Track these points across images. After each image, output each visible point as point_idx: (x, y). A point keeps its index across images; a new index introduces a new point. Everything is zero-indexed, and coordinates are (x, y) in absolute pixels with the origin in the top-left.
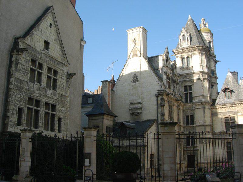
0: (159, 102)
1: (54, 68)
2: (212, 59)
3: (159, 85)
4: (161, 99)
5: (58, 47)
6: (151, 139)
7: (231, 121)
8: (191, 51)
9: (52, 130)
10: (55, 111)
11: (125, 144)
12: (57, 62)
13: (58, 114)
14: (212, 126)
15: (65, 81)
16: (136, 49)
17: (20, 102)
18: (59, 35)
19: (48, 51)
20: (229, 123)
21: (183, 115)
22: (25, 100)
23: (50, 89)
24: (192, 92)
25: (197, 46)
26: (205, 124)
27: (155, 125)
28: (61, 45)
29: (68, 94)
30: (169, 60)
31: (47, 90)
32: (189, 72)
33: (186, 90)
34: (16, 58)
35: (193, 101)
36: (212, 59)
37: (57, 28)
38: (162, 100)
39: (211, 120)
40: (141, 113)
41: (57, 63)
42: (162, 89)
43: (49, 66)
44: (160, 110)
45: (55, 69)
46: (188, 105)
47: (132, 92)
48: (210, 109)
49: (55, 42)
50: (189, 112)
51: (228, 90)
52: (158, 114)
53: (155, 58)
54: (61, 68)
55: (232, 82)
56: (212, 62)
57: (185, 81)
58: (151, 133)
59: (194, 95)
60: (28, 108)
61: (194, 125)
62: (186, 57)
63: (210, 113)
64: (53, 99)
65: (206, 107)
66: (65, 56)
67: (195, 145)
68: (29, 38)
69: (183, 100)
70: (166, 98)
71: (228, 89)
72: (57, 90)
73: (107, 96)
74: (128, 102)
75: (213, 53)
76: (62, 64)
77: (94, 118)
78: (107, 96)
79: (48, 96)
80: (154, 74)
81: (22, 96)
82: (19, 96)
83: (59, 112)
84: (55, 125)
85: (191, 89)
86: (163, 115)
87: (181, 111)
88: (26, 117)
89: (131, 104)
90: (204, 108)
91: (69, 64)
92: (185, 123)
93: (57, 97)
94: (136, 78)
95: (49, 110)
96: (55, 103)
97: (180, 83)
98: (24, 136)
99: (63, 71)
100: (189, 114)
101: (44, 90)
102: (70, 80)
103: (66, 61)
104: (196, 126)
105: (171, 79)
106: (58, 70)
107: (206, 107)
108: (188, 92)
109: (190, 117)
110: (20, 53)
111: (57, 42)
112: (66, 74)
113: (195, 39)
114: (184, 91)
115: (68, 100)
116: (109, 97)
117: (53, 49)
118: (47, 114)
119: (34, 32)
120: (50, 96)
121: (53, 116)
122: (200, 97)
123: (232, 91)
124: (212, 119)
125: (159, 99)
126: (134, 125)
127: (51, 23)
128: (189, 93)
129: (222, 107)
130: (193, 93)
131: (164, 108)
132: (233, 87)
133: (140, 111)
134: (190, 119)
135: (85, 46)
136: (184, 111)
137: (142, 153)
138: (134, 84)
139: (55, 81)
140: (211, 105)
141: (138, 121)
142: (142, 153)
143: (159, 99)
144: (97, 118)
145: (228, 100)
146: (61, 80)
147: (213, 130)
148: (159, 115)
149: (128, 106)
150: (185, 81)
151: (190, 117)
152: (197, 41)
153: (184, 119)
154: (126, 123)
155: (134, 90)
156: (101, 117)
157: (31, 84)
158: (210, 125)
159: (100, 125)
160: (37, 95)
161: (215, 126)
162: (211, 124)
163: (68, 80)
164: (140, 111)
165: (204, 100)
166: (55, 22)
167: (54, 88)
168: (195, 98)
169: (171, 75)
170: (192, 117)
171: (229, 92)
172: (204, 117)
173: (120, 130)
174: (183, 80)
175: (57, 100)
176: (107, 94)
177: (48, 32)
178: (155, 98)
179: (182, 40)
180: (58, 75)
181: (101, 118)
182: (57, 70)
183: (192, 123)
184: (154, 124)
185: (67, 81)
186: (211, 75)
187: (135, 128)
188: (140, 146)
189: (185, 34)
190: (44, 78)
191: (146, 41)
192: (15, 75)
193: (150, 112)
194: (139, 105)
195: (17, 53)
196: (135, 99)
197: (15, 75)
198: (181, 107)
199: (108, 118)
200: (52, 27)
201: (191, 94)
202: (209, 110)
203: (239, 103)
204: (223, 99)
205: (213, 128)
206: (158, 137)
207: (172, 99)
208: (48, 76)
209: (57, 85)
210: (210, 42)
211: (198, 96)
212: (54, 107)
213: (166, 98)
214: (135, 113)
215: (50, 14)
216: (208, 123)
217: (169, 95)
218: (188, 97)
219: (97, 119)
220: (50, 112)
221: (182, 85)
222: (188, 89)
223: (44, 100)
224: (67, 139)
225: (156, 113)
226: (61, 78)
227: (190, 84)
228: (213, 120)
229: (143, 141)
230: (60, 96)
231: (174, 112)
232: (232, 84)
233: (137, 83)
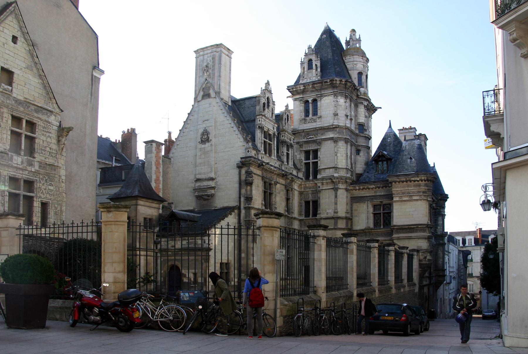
0: (243, 178)
1: (25, 118)
2: (362, 103)
3: (244, 148)
4: (247, 172)
5: (34, 81)
6: (228, 235)
7: (383, 210)
10: (33, 192)
12: (33, 108)
13: (40, 197)
14: (349, 219)
15: (54, 141)
16: (209, 85)
18: (36, 59)
19: (10, 88)
20: (380, 213)
21: (300, 200)
23: (20, 155)
24: (317, 162)
26: (335, 215)
27: (232, 216)
28: (42, 76)
29: (61, 162)
30: (271, 104)
31: (12, 156)
32: (315, 127)
33: (307, 158)
35: (319, 177)
36: (362, 103)
38: (249, 174)
39: (349, 211)
40: (212, 196)
41: (33, 109)
43: (14, 114)
44: (243, 191)
45: (27, 119)
46: (310, 184)
48: (347, 190)
49: (27, 70)
50: (310, 195)
52: (240, 198)
53: (246, 101)
54: (44, 117)
55: (394, 144)
57: (307, 142)
59: (321, 166)
61: (318, 217)
62: (310, 100)
63: (347, 197)
65: (341, 186)
66: (51, 96)
69: (301, 175)
70: (253, 169)
72: (36, 155)
73: (154, 168)
74: (192, 177)
75: (366, 94)
76: (44, 111)
78: (154, 168)
79: (16, 165)
80: (237, 131)
83: (42, 193)
84: (34, 214)
85: (316, 156)
86: (249, 199)
87: (296, 193)
89: (198, 180)
90: (336, 189)
91: (62, 111)
92: (303, 213)
93: (37, 167)
94: (206, 137)
95: (19, 190)
96: (31, 178)
97: (295, 146)
100: (310, 198)
101: (5, 155)
102: (64, 139)
103: (55, 105)
104: (321, 219)
105: (274, 137)
106: (35, 120)
107: (341, 186)
108: (311, 161)
109: (311, 204)
111: (32, 70)
112: (56, 128)
114: (303, 159)
115: (63, 172)
116: (157, 168)
117: (23, 84)
120: (20, 166)
121: (29, 200)
122: (331, 170)
124: (352, 208)
125: (243, 171)
126: (198, 215)
127: (15, 35)
128: (313, 163)
130: (319, 162)
131: (251, 187)
132: (393, 153)
133: (213, 191)
134: (311, 207)
135: (103, 79)
136: (301, 193)
138: (203, 146)
139: (31, 140)
140: (351, 184)
141: (208, 209)
143: (243, 171)
145: (382, 177)
146: (45, 139)
147: (352, 225)
148: (242, 199)
151: (311, 204)
153: (300, 206)
154: (181, 212)
155: (203, 156)
156: (134, 202)
158: (346, 218)
161: (355, 219)
162: (349, 216)
164: (213, 191)
165: (336, 175)
166: (25, 34)
167: (31, 151)
169: (275, 130)
170: (316, 204)
172: (336, 204)
173: (170, 223)
174: (304, 140)
175: (37, 173)
176: (153, 163)
177: (7, 52)
178: (236, 171)
180: (37, 130)
181: (134, 204)
182: (34, 122)
183: (315, 214)
184: (231, 214)
185: (59, 141)
186: (357, 132)
188: (202, 249)
191: (230, 70)
193: (227, 195)
196: (204, 172)
198: (296, 187)
199: (148, 204)
200: (19, 43)
201: (316, 164)
202: (345, 193)
204: (373, 174)
205: (352, 222)
207: (273, 173)
208: (13, 132)
209: (36, 147)
212: (29, 184)
213: (253, 169)
214: (204, 196)
215: (10, 18)
216: (342, 213)
217: (262, 165)
218: (311, 170)
220: (22, 192)
221: (301, 149)
222: (311, 156)
224: (47, 235)
225: (238, 196)
226: (43, 135)
227: (308, 149)
228: (353, 209)
230: (42, 165)
231: (278, 195)
232: (392, 149)
233: (207, 144)
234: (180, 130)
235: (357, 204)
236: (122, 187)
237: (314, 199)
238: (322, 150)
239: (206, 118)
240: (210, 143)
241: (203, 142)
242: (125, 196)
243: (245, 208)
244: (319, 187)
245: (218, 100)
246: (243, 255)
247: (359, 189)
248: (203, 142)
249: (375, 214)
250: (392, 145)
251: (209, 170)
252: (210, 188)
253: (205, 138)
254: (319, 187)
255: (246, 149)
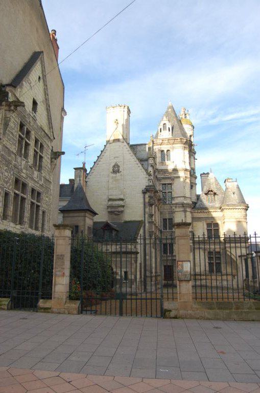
0: (147, 200)
8: (173, 144)
9: (36, 229)
11: (110, 250)
15: (49, 161)
17: (7, 183)
20: (211, 230)
21: (161, 217)
22: (12, 181)
25: (181, 139)
34: (5, 116)
36: (192, 155)
37: (45, 85)
40: (122, 212)
42: (151, 184)
44: (147, 210)
47: (111, 186)
48: (191, 212)
51: (212, 193)
52: (145, 215)
56: (192, 159)
58: (255, 234)
60: (16, 195)
64: (38, 185)
65: (188, 210)
66: (51, 126)
67: (174, 254)
68: (19, 90)
71: (212, 191)
74: (105, 197)
77: (71, 215)
81: (10, 175)
82: (6, 174)
88: (12, 207)
89: (110, 200)
90: (185, 211)
91: (54, 138)
98: (63, 235)
99: (49, 146)
100: (167, 217)
110: (12, 108)
113: (177, 129)
118: (32, 203)
119: (24, 83)
123: (215, 194)
125: (147, 196)
129: (237, 207)
130: (173, 193)
137: (133, 262)
138: (115, 175)
140: (192, 208)
142: (133, 262)
144: (77, 214)
148: (147, 216)
149: (106, 203)
150: (163, 178)
152: (180, 133)
155: (114, 182)
156: (82, 214)
157: (19, 159)
159: (81, 224)
160: (24, 175)
163: (53, 160)
165: (185, 202)
166: (44, 76)
168: (175, 199)
171: (213, 195)
174: (163, 176)
175: (42, 186)
178: (142, 195)
179: (162, 129)
185: (52, 162)
187: (116, 230)
188: (131, 253)
189: (167, 122)
190: (31, 153)
192: (4, 141)
194: (121, 202)
195: (7, 108)
196: (116, 194)
197: (4, 141)
203: (227, 207)
206: (145, 242)
210: (190, 136)
211: (179, 197)
214: (115, 210)
219: (76, 216)
223: (31, 184)
229: (135, 247)
234: (95, 163)
235: (196, 222)
236: (69, 202)
237: (170, 218)
238: (175, 184)
239: (117, 156)
240: (120, 174)
241: (114, 172)
242: (75, 209)
243: (149, 222)
244: (174, 209)
245: (125, 144)
246: (147, 257)
247: (197, 212)
248: (114, 172)
249: (208, 230)
250: (214, 184)
251: (120, 193)
252: (121, 206)
253: (116, 169)
254: (174, 209)
255: (149, 180)
